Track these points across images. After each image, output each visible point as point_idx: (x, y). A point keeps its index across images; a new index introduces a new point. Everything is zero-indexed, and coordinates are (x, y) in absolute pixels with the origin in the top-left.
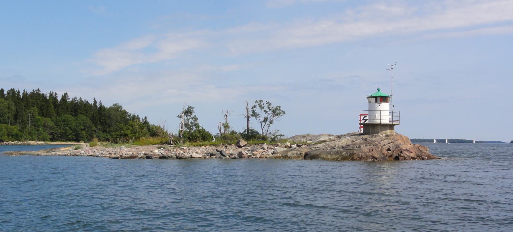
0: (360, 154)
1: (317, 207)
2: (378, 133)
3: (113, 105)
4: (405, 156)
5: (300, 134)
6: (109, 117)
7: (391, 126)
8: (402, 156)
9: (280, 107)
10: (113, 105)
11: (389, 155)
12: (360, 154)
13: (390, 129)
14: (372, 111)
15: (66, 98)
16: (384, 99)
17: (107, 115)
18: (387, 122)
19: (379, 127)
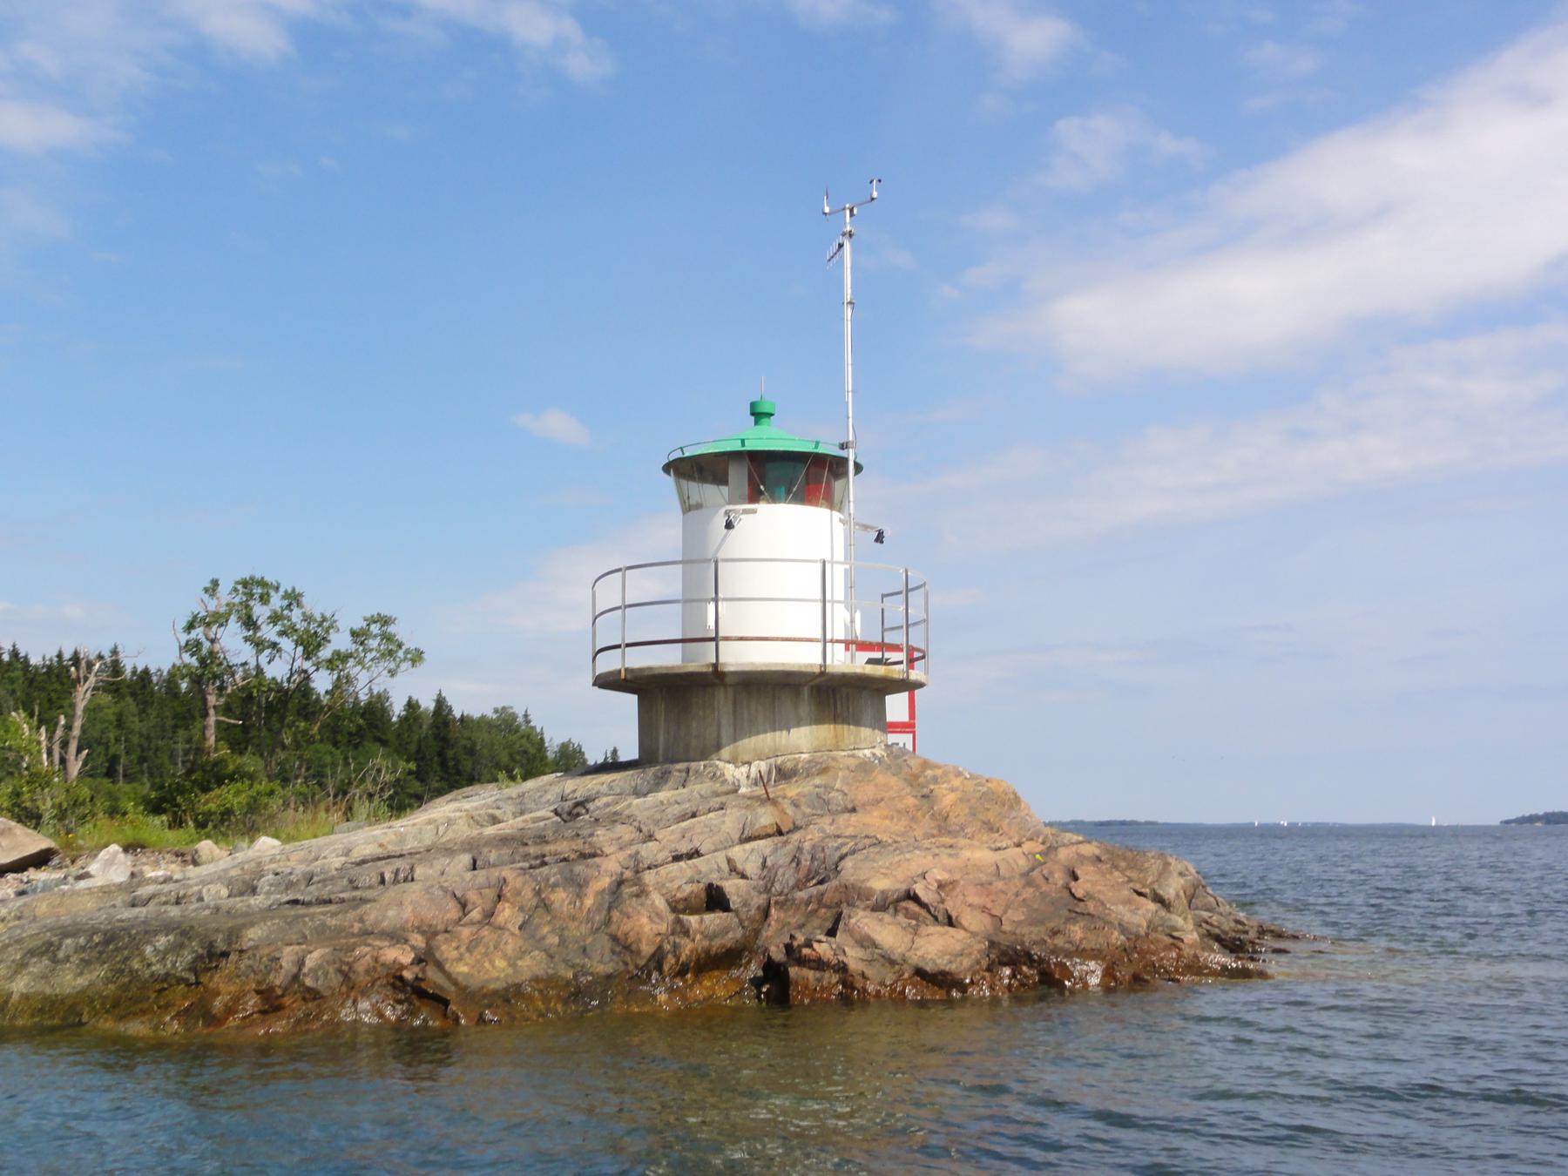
0: (288, 956)
1: (1018, 1122)
2: (709, 750)
3: (496, 711)
4: (854, 958)
5: (1519, 815)
6: (471, 751)
7: (837, 697)
8: (819, 964)
9: (385, 621)
10: (496, 711)
11: (687, 948)
12: (288, 956)
13: (818, 720)
14: (701, 572)
15: (307, 685)
16: (806, 475)
17: (463, 742)
18: (804, 657)
19: (722, 700)
